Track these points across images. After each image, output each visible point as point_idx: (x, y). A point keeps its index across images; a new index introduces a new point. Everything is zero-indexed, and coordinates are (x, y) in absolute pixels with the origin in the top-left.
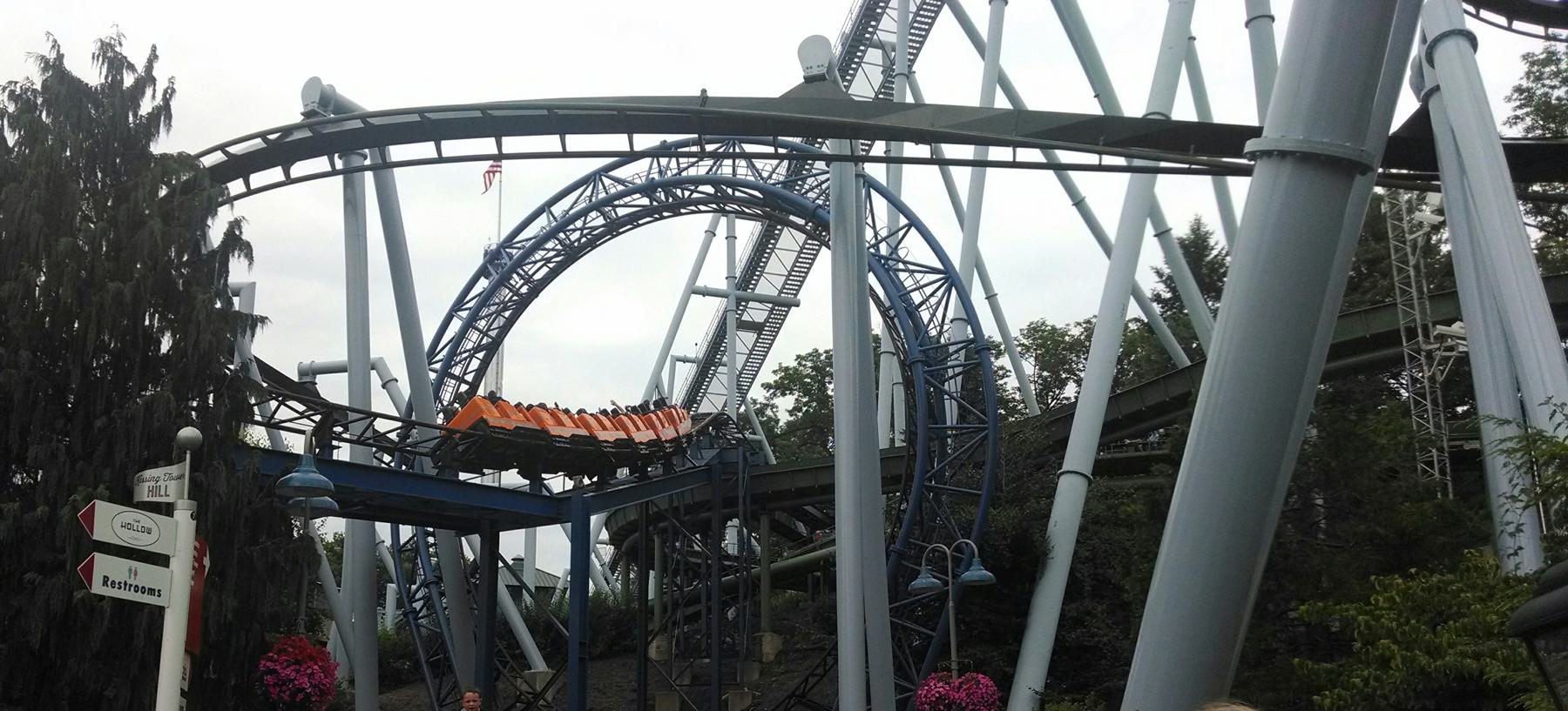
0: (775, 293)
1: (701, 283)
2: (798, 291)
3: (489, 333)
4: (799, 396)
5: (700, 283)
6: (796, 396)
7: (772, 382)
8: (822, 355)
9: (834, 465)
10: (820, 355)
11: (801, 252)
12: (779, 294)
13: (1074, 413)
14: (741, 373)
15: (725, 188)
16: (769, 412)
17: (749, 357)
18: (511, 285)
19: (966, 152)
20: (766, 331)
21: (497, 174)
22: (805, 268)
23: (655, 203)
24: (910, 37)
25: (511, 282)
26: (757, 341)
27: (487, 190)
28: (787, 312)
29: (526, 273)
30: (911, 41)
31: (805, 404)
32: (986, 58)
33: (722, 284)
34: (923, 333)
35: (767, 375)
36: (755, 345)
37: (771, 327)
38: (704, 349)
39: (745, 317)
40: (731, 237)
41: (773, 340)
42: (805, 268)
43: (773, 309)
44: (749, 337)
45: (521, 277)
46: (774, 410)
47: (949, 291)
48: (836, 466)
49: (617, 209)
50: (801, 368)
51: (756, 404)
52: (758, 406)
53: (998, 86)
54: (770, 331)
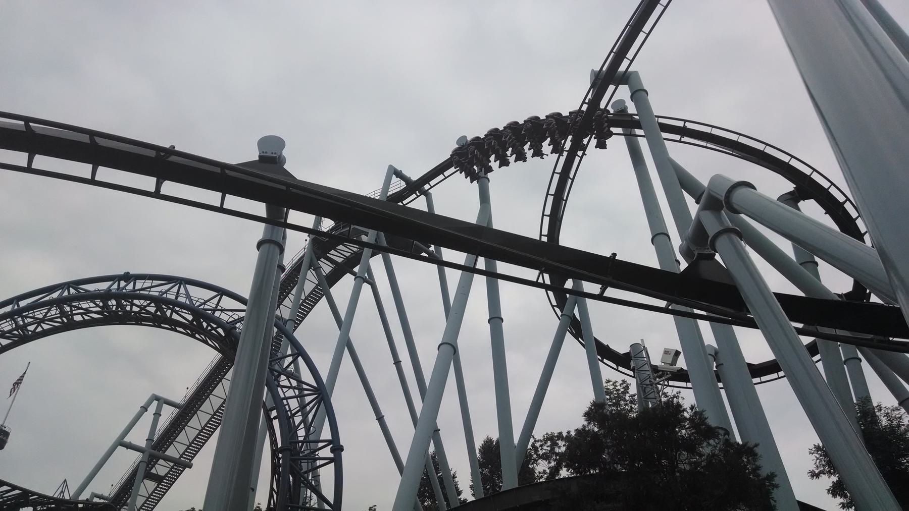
0: (177, 456)
1: (128, 439)
2: (193, 458)
5: (127, 439)
12: (180, 458)
15: (202, 320)
17: (147, 500)
19: (458, 257)
22: (152, 505)
23: (159, 313)
26: (156, 489)
28: (182, 471)
30: (299, 312)
33: (143, 444)
39: (153, 471)
40: (157, 414)
41: (167, 490)
42: (152, 505)
43: (172, 467)
44: (151, 485)
49: (134, 307)
54: (167, 483)
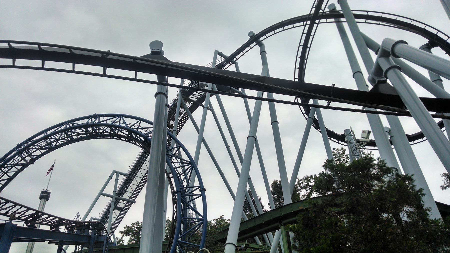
0: (128, 198)
2: (135, 198)
3: (7, 173)
4: (131, 237)
5: (104, 192)
6: (130, 237)
7: (123, 231)
8: (140, 223)
9: (139, 247)
10: (140, 223)
11: (138, 186)
12: (129, 199)
13: (229, 228)
14: (113, 224)
16: (121, 242)
18: (22, 156)
20: (124, 211)
21: (52, 170)
24: (178, 127)
25: (23, 155)
26: (120, 214)
27: (47, 175)
28: (131, 205)
29: (29, 152)
30: (178, 128)
31: (133, 240)
32: (199, 133)
33: (112, 193)
34: (181, 183)
35: (121, 227)
36: (119, 215)
37: (126, 210)
38: (102, 215)
39: (118, 206)
40: (117, 180)
43: (127, 203)
44: (117, 212)
45: (27, 153)
46: (123, 242)
47: (192, 169)
48: (140, 248)
50: (133, 228)
51: (118, 239)
52: (118, 240)
53: (202, 142)
